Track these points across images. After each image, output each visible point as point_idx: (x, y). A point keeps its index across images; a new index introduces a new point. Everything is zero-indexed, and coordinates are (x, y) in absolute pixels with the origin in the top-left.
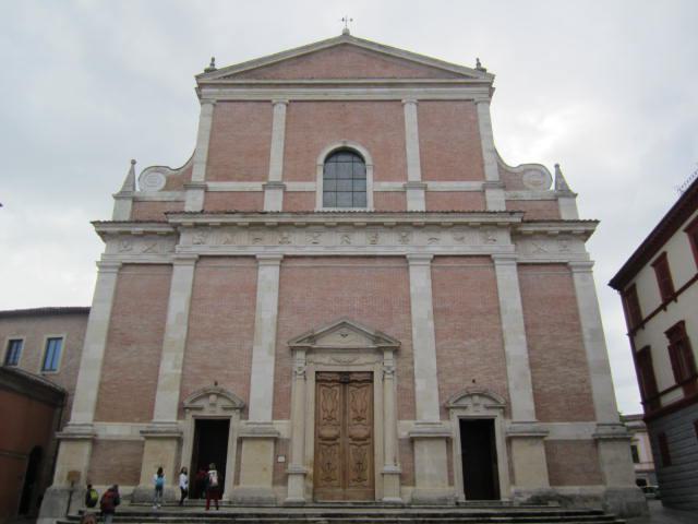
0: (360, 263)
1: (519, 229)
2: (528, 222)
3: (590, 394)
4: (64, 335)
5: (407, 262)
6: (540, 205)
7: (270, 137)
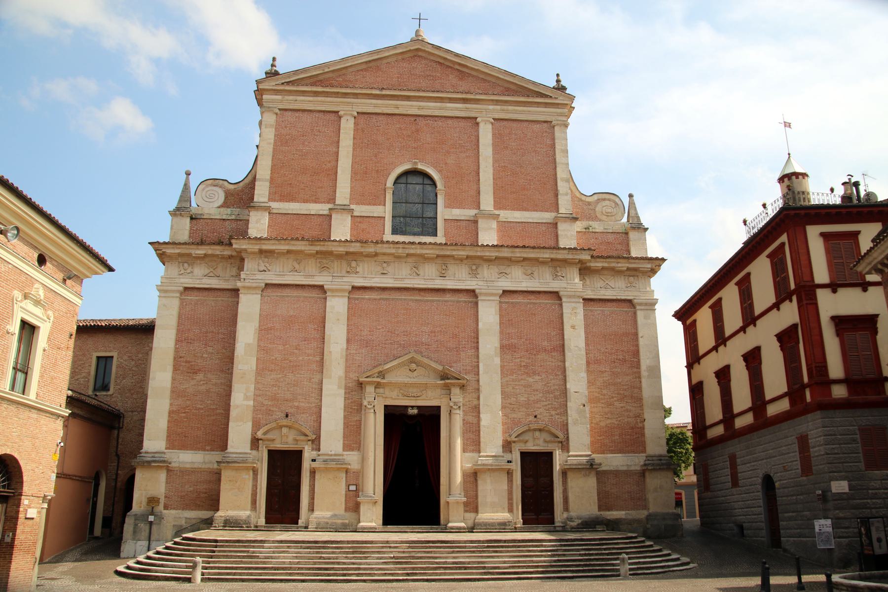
0: (429, 297)
1: (588, 264)
3: (643, 428)
4: (114, 354)
6: (611, 238)
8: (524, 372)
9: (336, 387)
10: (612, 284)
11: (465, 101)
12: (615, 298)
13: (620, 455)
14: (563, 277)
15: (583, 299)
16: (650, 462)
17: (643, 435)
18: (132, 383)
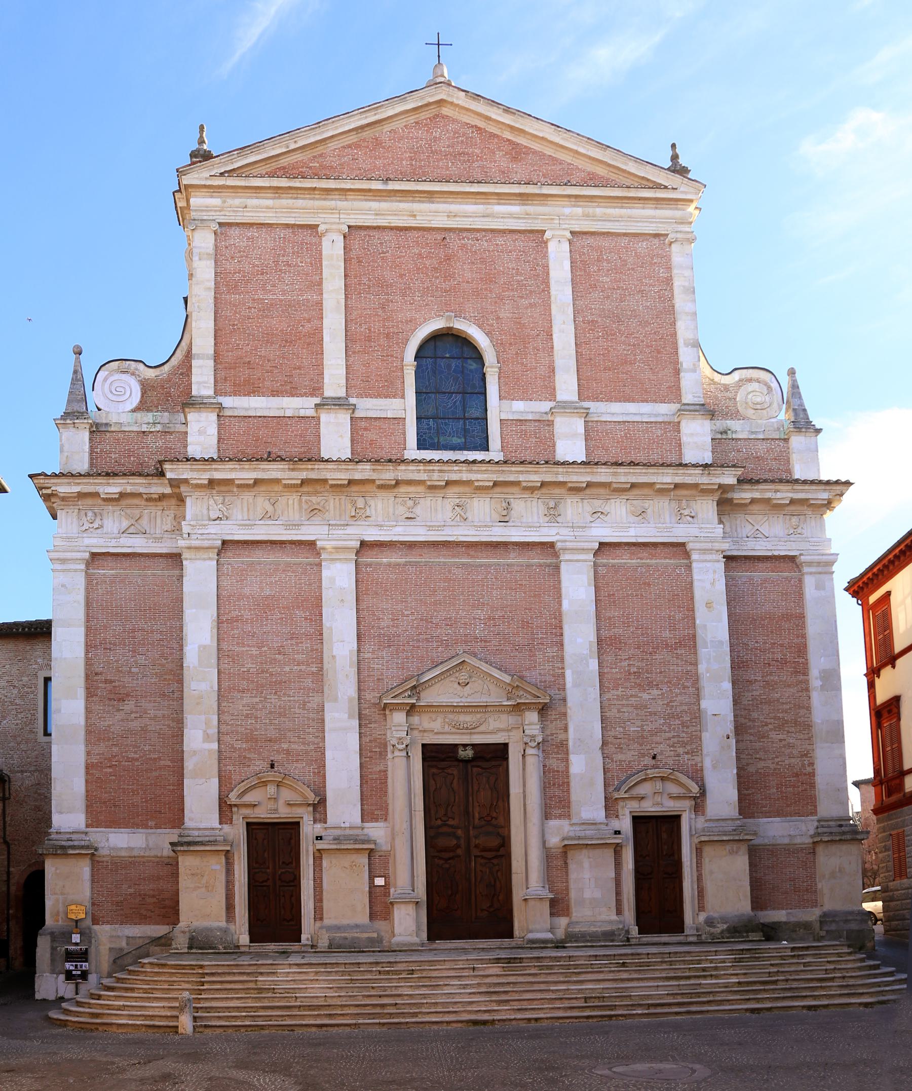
1: (729, 496)
2: (750, 481)
3: (812, 774)
5: (319, 554)
6: (762, 447)
7: (320, 304)
8: (635, 683)
9: (346, 716)
11: (523, 198)
12: (770, 554)
13: (778, 819)
14: (693, 517)
16: (825, 830)
17: (813, 785)
18: (17, 724)
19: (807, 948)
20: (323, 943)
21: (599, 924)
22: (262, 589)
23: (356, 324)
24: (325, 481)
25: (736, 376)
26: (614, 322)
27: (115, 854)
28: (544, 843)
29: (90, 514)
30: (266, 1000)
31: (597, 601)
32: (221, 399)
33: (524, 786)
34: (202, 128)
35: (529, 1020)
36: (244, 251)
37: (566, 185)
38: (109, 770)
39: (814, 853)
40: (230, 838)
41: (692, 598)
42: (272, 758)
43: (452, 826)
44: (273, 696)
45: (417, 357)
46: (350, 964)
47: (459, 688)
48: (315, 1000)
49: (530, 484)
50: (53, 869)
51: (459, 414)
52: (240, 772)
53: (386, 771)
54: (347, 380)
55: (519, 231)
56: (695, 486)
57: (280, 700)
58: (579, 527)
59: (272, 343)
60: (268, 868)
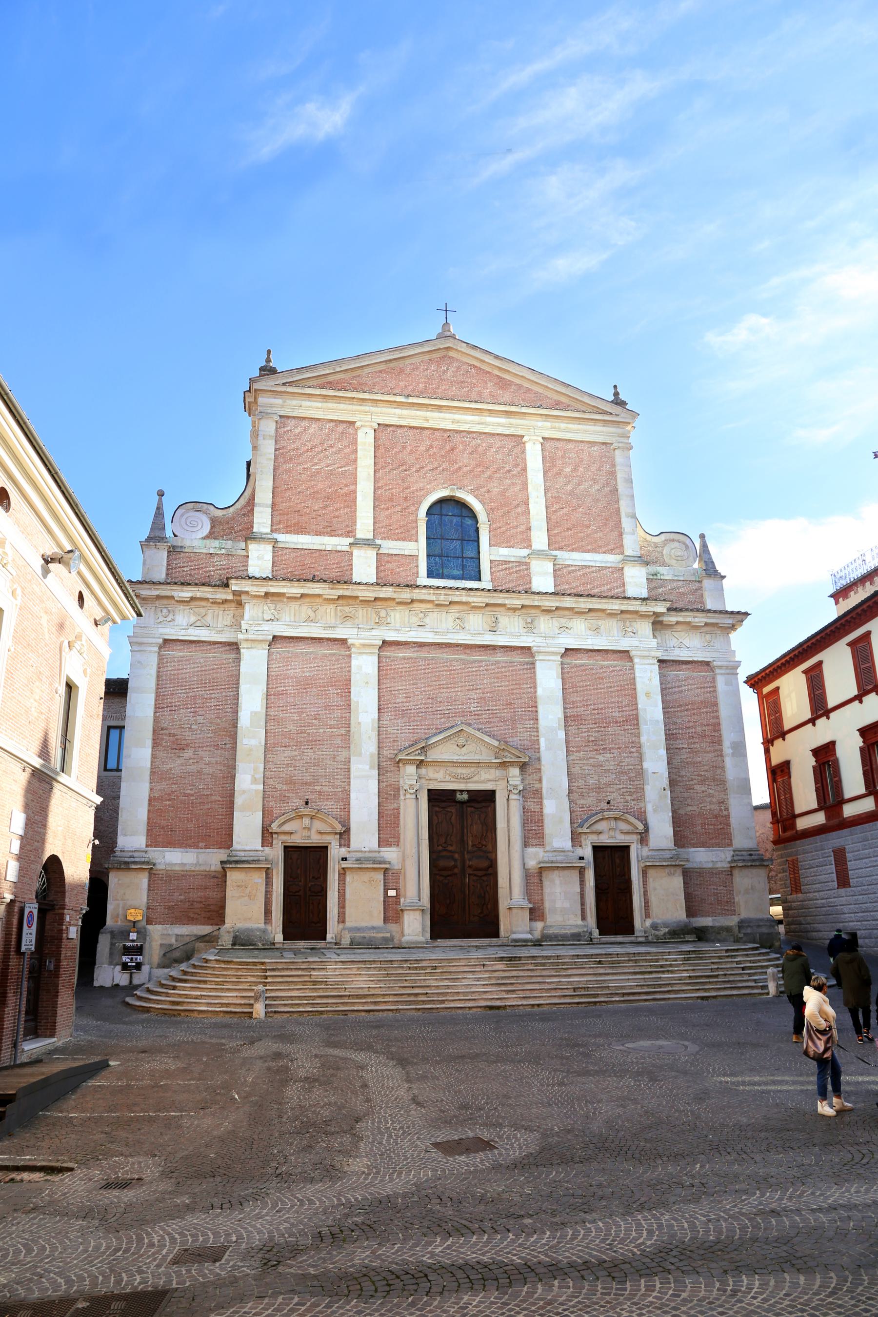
1: (660, 619)
2: (676, 610)
3: (728, 817)
6: (682, 587)
7: (354, 475)
9: (368, 767)
10: (687, 642)
11: (508, 414)
12: (691, 659)
15: (659, 661)
17: (728, 825)
19: (737, 950)
20: (346, 941)
21: (568, 927)
22: (303, 672)
23: (382, 489)
24: (357, 597)
25: (663, 537)
26: (574, 499)
27: (169, 869)
28: (524, 865)
29: (165, 611)
30: (321, 991)
31: (564, 689)
32: (276, 536)
33: (508, 822)
34: (269, 352)
35: (533, 1005)
36: (298, 436)
37: (538, 407)
38: (168, 803)
39: (731, 874)
40: (270, 858)
41: (635, 690)
42: (307, 797)
43: (450, 851)
44: (309, 751)
45: (428, 514)
46: (385, 961)
47: (458, 748)
48: (360, 990)
49: (513, 606)
50: (116, 880)
51: (459, 554)
52: (280, 807)
53: (398, 809)
54: (374, 527)
55: (505, 435)
56: (636, 612)
57: (314, 753)
58: (550, 637)
59: (317, 499)
60: (301, 881)
